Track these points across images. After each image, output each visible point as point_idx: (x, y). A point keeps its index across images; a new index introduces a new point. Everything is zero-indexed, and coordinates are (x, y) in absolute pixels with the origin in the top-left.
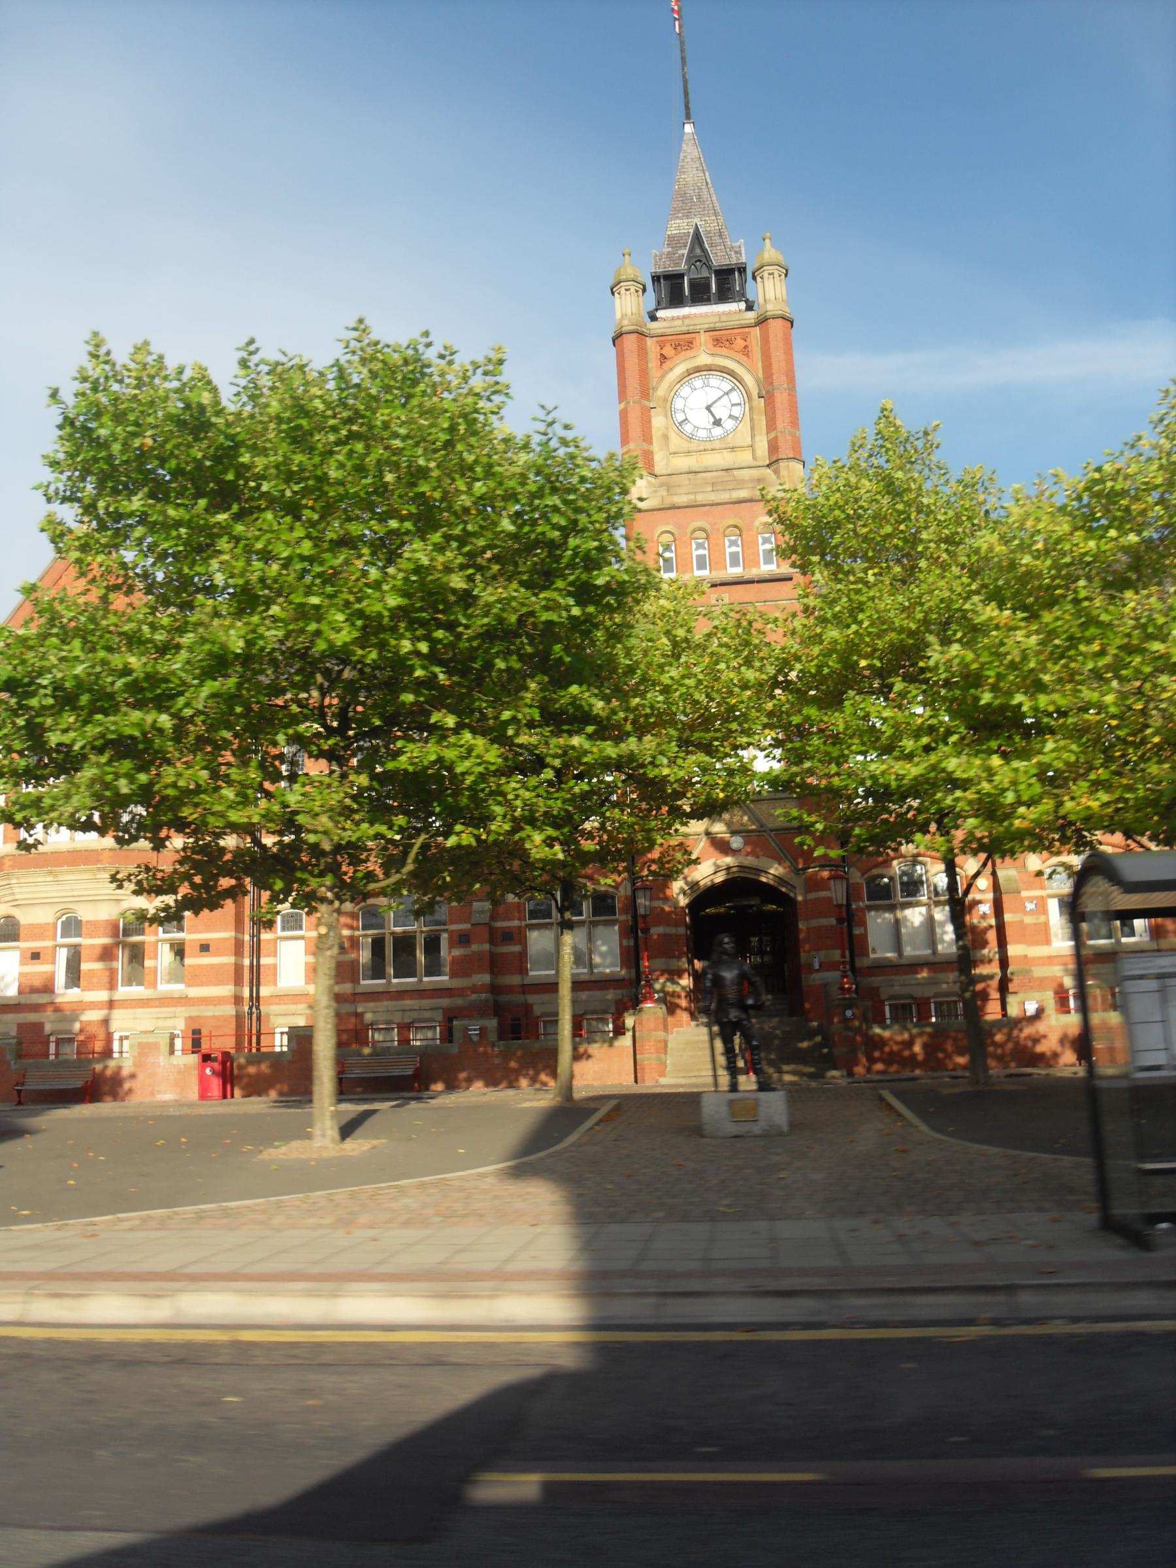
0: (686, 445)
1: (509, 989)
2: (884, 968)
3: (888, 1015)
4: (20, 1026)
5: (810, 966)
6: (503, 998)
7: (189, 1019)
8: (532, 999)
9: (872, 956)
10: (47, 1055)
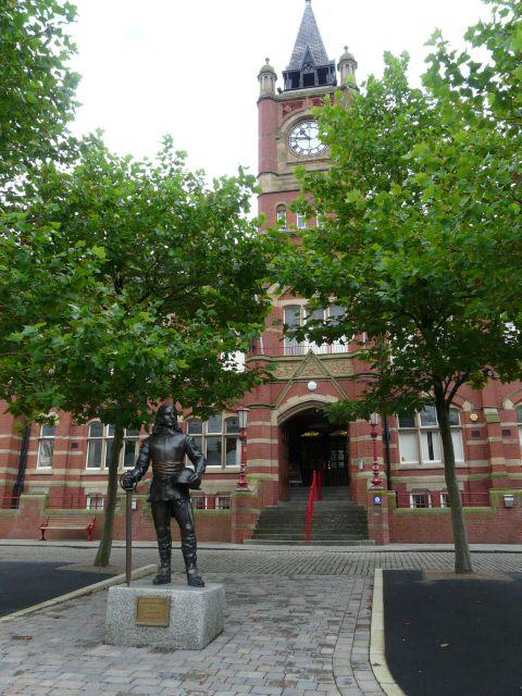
0: (296, 160)
2: (406, 471)
3: (88, 504)
5: (357, 467)
8: (84, 483)
9: (402, 463)
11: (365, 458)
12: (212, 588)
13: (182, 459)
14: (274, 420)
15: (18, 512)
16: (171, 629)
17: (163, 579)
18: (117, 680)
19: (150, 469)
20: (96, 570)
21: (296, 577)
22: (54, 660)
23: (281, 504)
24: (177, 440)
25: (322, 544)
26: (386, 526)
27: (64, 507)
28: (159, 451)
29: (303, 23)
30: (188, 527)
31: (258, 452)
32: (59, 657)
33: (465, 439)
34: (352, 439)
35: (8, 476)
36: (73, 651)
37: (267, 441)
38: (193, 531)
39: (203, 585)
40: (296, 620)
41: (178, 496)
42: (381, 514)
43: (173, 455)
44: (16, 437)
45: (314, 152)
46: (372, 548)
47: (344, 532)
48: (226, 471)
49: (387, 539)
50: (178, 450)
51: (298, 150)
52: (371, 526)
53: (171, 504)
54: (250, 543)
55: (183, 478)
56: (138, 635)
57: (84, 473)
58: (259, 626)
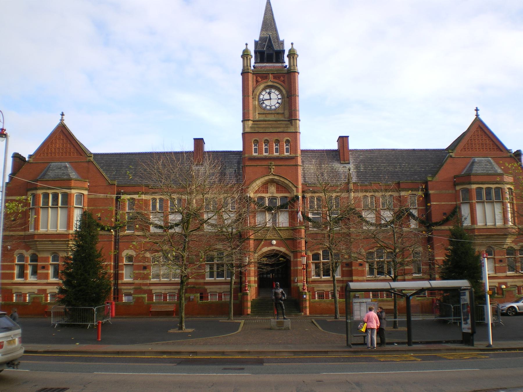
5: (294, 281)
29: (265, 14)
33: (342, 267)
45: (273, 107)
51: (264, 105)
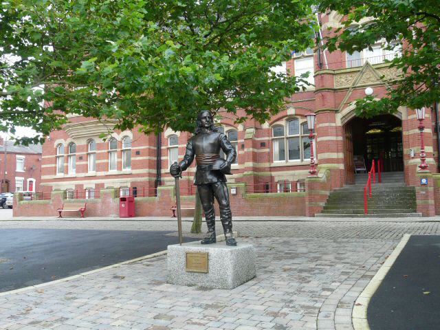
1: (263, 170)
3: (278, 188)
4: (76, 186)
5: (409, 156)
6: (260, 174)
7: (132, 183)
8: (273, 174)
10: (85, 197)
11: (415, 148)
12: (242, 246)
13: (218, 152)
14: (339, 121)
15: (157, 198)
16: (210, 274)
17: (210, 240)
18: (162, 306)
19: (194, 161)
20: (191, 235)
21: (339, 240)
22: (130, 291)
23: (346, 187)
24: (212, 138)
25: (377, 216)
26: (431, 202)
27: (189, 194)
28: (198, 147)
30: (224, 202)
31: (323, 147)
32: (135, 289)
34: (405, 133)
35: (150, 175)
36: (145, 286)
37: (334, 138)
38: (228, 206)
39: (235, 244)
40: (317, 271)
41: (215, 180)
42: (427, 192)
43: (209, 149)
44: (152, 148)
46: (418, 219)
47: (396, 208)
48: (303, 163)
49: (432, 211)
50: (213, 145)
52: (419, 202)
53: (211, 186)
54: (320, 216)
55: (217, 165)
56: (188, 278)
57: (272, 165)
58: (285, 275)
